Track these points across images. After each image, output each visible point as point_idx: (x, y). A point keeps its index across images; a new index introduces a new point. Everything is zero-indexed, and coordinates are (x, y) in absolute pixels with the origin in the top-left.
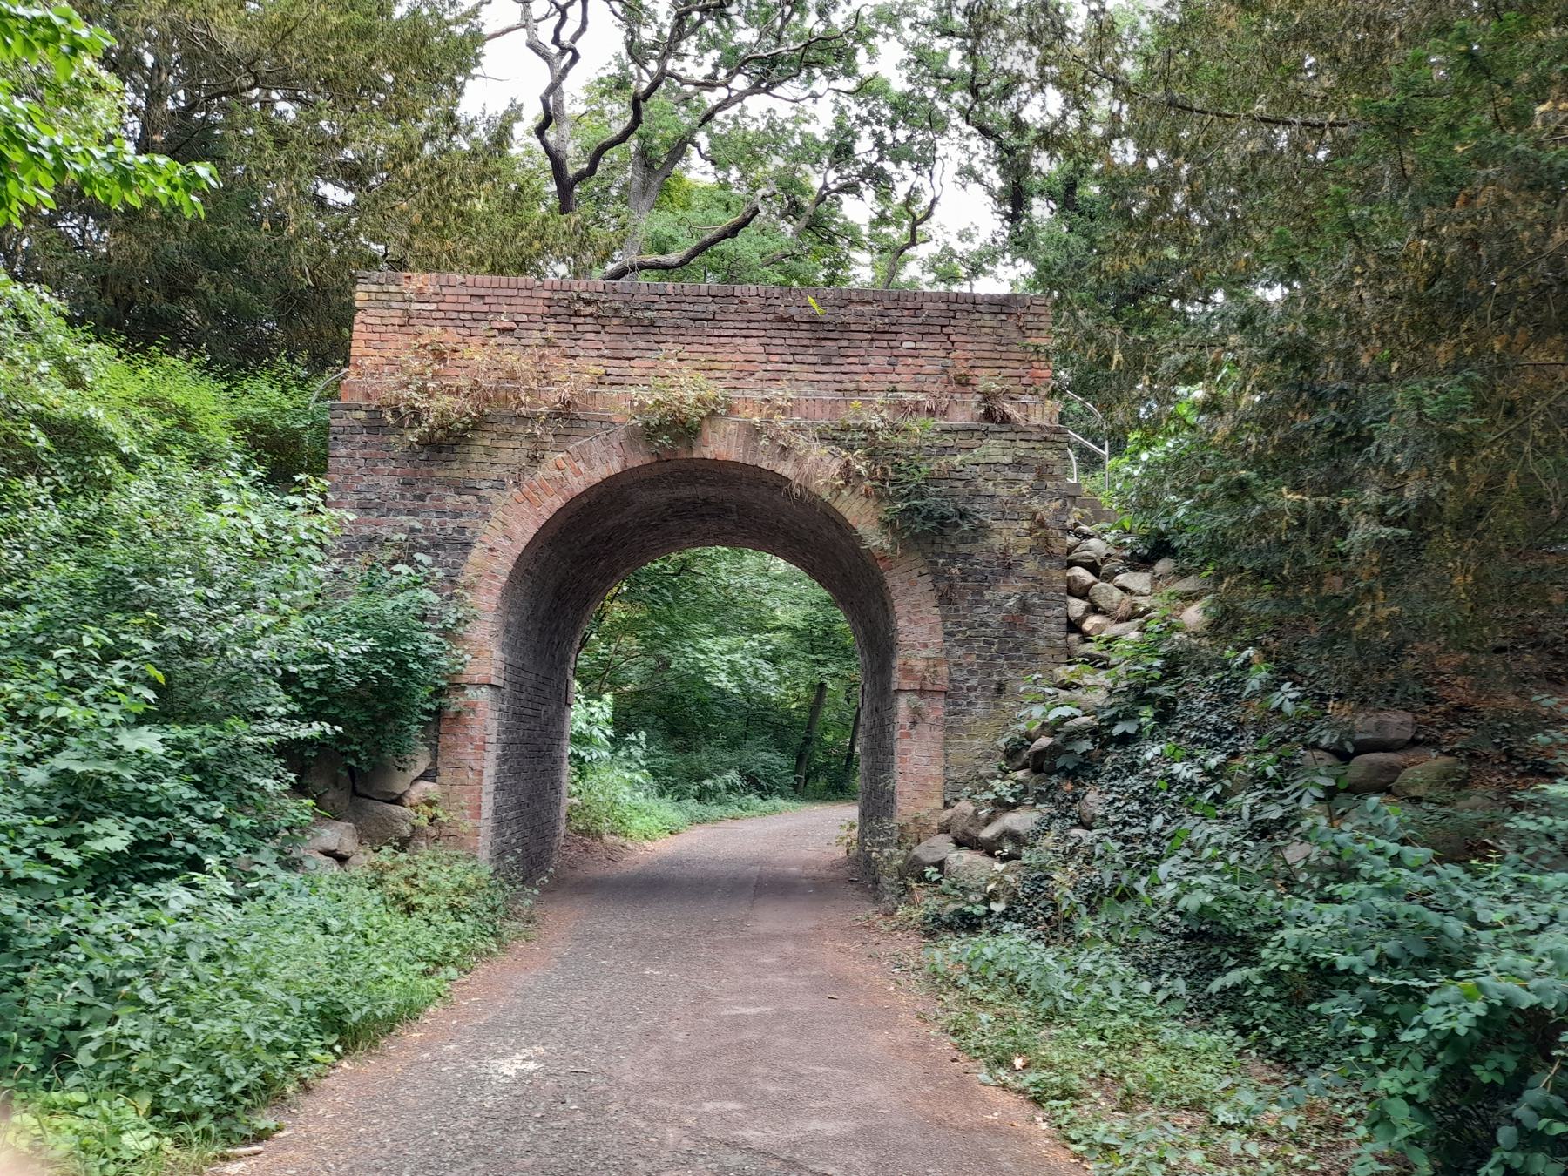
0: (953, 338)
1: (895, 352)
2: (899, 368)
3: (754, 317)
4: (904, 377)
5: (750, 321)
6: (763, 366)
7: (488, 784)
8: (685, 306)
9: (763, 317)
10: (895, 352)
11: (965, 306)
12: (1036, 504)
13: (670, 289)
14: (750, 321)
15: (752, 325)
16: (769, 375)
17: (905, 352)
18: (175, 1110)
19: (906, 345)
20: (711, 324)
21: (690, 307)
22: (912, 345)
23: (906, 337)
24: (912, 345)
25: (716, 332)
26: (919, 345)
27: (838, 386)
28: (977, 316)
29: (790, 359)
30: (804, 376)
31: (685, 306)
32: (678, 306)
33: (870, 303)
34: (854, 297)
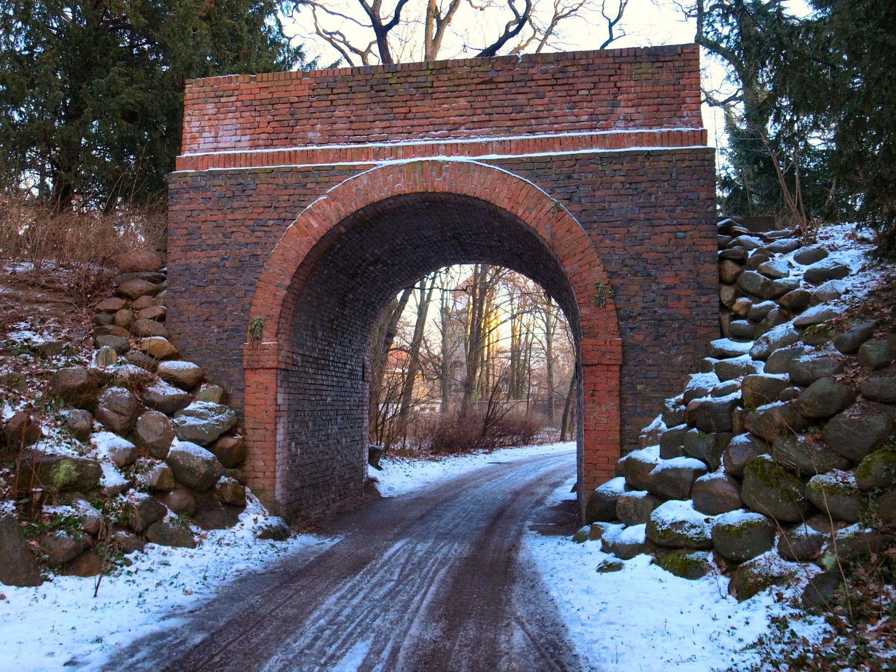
0: (619, 84)
3: (462, 82)
14: (459, 85)
15: (461, 88)
21: (414, 80)
22: (586, 92)
24: (586, 92)
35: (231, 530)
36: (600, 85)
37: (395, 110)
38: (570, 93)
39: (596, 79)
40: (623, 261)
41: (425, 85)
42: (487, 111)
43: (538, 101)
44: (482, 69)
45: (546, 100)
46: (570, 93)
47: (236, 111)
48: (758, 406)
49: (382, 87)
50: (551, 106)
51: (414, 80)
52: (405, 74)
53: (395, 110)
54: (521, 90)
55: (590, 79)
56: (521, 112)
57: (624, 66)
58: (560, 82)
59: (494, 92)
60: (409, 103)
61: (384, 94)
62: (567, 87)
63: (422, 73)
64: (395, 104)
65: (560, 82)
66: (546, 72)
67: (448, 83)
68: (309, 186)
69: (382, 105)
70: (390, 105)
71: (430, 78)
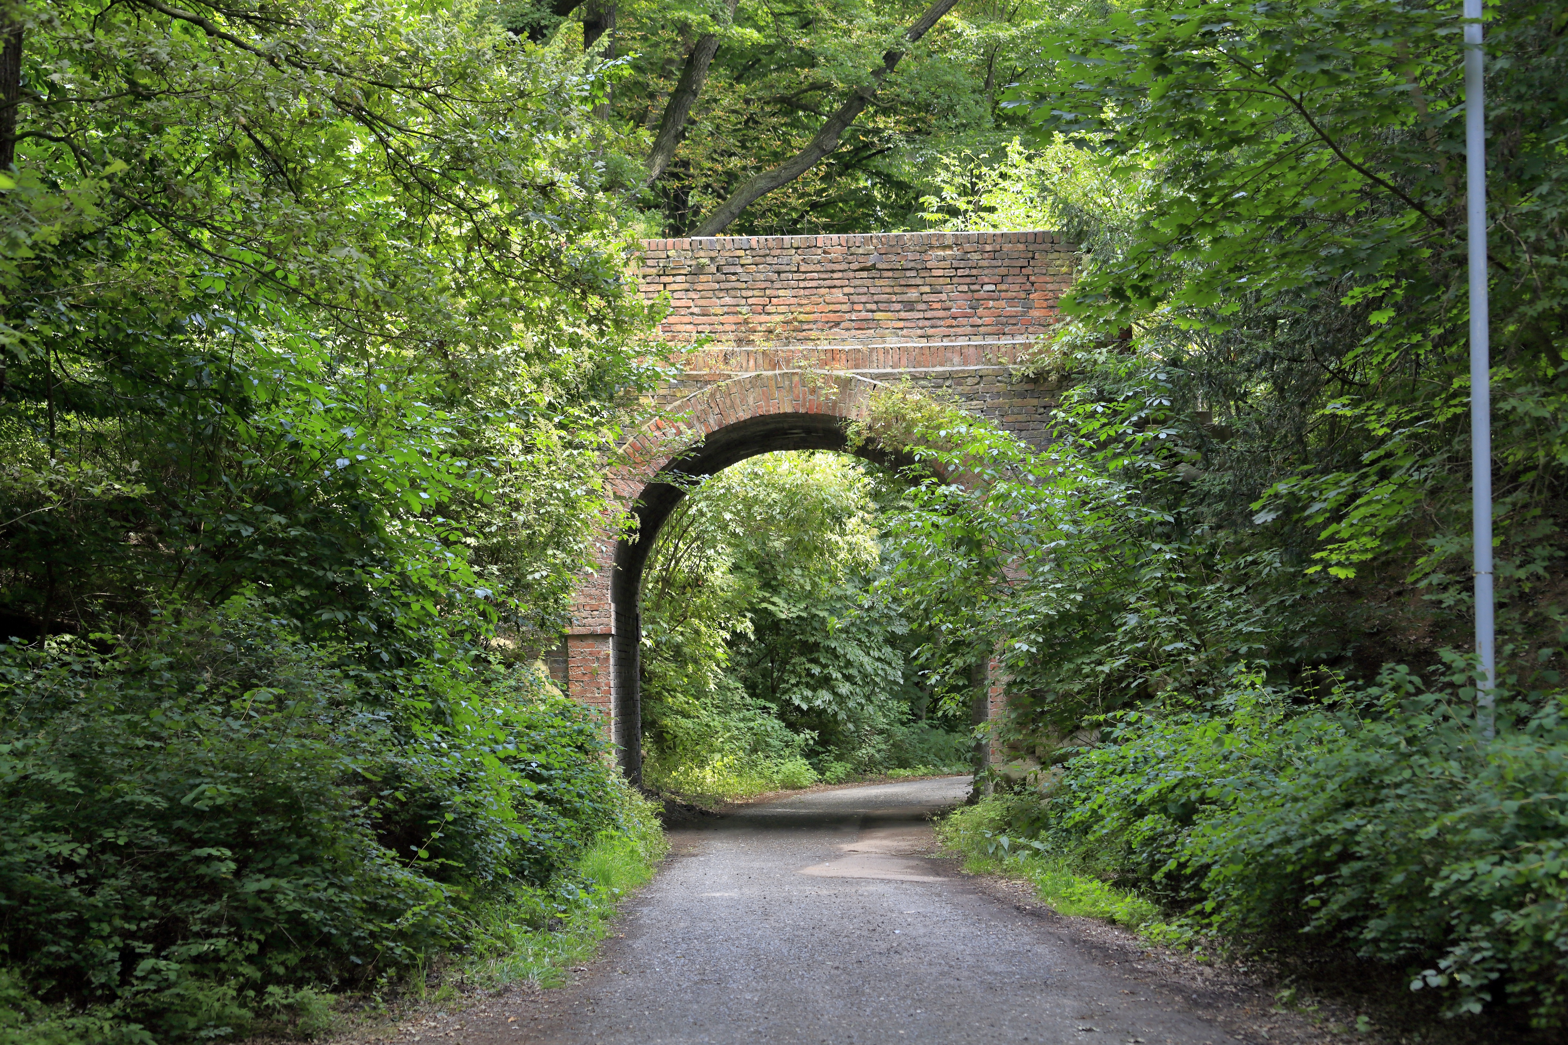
0: (1032, 278)
1: (976, 295)
2: (980, 311)
3: (836, 267)
4: (986, 320)
5: (833, 272)
6: (847, 316)
7: (612, 676)
8: (769, 260)
9: (846, 266)
10: (976, 295)
11: (1043, 246)
12: (183, 283)
13: (754, 244)
14: (833, 272)
15: (835, 275)
16: (725, 309)
17: (985, 295)
18: (52, 645)
19: (986, 288)
20: (796, 276)
21: (775, 260)
22: (993, 287)
23: (986, 280)
24: (993, 287)
25: (802, 284)
26: (999, 287)
27: (919, 332)
28: (1056, 255)
29: (874, 307)
30: (891, 324)
31: (769, 260)
32: (763, 260)
33: (950, 247)
34: (934, 242)
35: (79, 1022)
36: (1010, 279)
37: (750, 301)
38: (973, 287)
39: (1003, 271)
40: (1159, 52)
41: (787, 268)
42: (869, 306)
43: (932, 298)
44: (861, 251)
45: (944, 297)
46: (973, 287)
47: (357, 180)
48: (142, 499)
49: (732, 269)
50: (948, 304)
51: (775, 260)
52: (762, 252)
53: (750, 301)
54: (912, 282)
55: (996, 271)
56: (912, 310)
57: (1037, 255)
58: (960, 272)
59: (878, 282)
60: (768, 292)
61: (733, 278)
62: (968, 280)
63: (785, 252)
64: (750, 293)
65: (960, 272)
66: (944, 259)
67: (818, 267)
68: (1086, 670)
69: (733, 293)
70: (745, 293)
71: (798, 258)
